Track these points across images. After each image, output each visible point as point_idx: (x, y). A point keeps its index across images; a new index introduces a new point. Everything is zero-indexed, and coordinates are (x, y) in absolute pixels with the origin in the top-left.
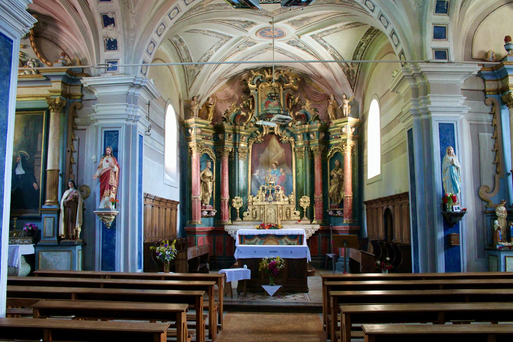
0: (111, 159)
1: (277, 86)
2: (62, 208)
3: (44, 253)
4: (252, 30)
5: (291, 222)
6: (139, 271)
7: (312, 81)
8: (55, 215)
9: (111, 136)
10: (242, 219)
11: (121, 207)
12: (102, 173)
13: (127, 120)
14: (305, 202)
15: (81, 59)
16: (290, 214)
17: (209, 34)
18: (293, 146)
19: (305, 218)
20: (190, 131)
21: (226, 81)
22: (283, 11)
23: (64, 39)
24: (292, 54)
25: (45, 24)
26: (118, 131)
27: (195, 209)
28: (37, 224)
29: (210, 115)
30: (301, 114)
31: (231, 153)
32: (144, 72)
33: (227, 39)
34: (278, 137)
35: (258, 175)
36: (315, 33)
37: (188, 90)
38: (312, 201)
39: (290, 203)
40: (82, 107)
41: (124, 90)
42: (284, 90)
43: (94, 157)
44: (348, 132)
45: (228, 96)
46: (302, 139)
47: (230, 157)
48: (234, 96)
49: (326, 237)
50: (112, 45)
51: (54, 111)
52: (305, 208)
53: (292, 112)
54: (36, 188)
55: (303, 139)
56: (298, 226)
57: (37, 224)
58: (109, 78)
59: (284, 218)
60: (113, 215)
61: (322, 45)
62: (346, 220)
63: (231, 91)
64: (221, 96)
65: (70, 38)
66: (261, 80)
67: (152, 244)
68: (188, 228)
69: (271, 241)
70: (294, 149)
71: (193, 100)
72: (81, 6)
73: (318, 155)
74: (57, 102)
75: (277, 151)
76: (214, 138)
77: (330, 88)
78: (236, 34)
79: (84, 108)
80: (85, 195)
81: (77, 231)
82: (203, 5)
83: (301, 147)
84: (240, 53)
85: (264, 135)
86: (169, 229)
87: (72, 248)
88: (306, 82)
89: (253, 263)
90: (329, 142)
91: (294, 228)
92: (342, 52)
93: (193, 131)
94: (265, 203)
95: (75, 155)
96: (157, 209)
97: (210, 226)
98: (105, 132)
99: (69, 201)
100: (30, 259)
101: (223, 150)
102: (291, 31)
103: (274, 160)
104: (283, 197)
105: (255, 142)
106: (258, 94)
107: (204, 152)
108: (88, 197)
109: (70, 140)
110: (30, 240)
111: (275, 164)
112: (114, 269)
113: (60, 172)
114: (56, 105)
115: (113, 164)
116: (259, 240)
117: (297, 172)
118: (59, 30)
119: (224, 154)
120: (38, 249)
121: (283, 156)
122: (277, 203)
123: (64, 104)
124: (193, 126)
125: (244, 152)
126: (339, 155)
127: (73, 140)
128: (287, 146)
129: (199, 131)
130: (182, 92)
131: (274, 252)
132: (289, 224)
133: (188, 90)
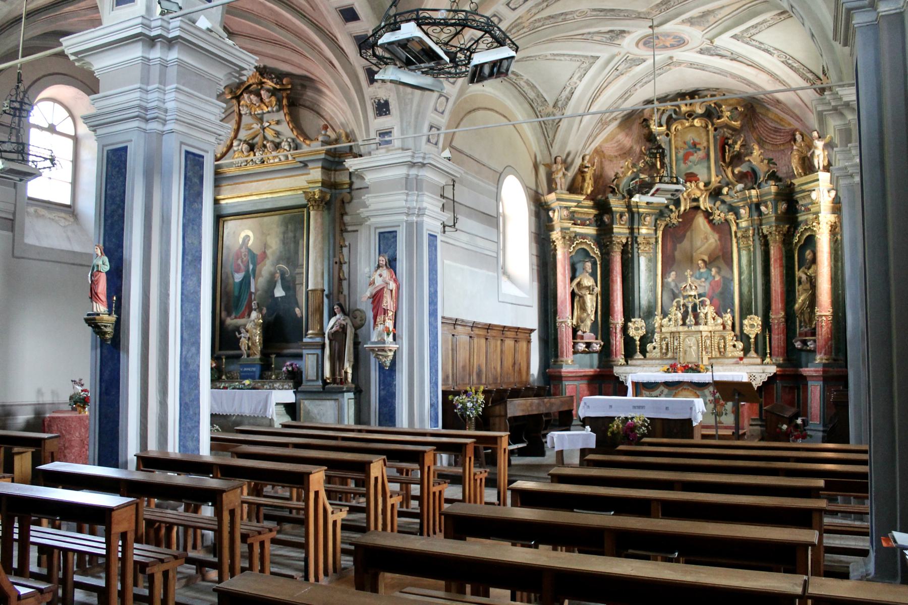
0: (385, 272)
1: (704, 125)
2: (327, 342)
3: (306, 402)
4: (628, 44)
5: (726, 361)
6: (439, 429)
7: (768, 109)
8: (319, 352)
9: (388, 239)
10: (645, 356)
11: (402, 339)
12: (374, 292)
13: (408, 215)
14: (752, 326)
15: (348, 131)
16: (725, 346)
17: (557, 58)
18: (734, 228)
19: (752, 353)
20: (551, 213)
21: (616, 123)
22: (664, 7)
23: (328, 104)
24: (715, 68)
25: (304, 87)
26: (396, 232)
27: (562, 341)
28: (298, 363)
29: (586, 185)
30: (745, 171)
31: (625, 245)
32: (433, 141)
33: (592, 61)
34: (708, 214)
35: (673, 280)
36: (737, 30)
37: (549, 146)
38: (766, 324)
39: (724, 328)
40: (352, 199)
41: (402, 171)
42: (716, 129)
43: (367, 270)
44: (821, 200)
45: (621, 149)
46: (747, 215)
47: (624, 252)
48: (632, 147)
49: (791, 388)
50: (382, 108)
51: (313, 209)
52: (752, 336)
53: (730, 169)
54: (299, 315)
55: (751, 215)
56: (737, 367)
57: (298, 363)
58: (381, 157)
59: (715, 353)
60: (390, 350)
61: (759, 48)
62: (820, 358)
63: (627, 140)
64: (610, 149)
65: (335, 102)
66: (674, 116)
67: (450, 393)
68: (551, 370)
69: (685, 393)
70: (736, 233)
71: (555, 163)
72: (337, 59)
73: (775, 241)
74: (317, 197)
75: (706, 238)
76: (596, 221)
77: (798, 118)
78: (604, 52)
79: (355, 201)
80: (359, 323)
81: (346, 373)
82: (521, 23)
83: (747, 229)
84: (623, 78)
85: (681, 212)
86: (511, 371)
87: (339, 396)
88: (758, 110)
89: (599, 424)
90: (797, 218)
91: (731, 370)
92: (800, 55)
93: (556, 214)
94: (681, 329)
95: (345, 268)
96: (483, 341)
97: (592, 367)
98: (380, 233)
99: (336, 332)
100: (291, 409)
101: (611, 242)
102: (696, 35)
103: (701, 253)
104: (714, 319)
105: (666, 225)
106: (670, 141)
107: (580, 247)
108: (362, 325)
109: (337, 248)
110: (291, 384)
111: (703, 261)
112: (394, 425)
113: (326, 292)
114: (315, 201)
115: (387, 280)
116: (666, 391)
117: (740, 274)
118: (319, 91)
119: (612, 248)
120: (299, 396)
121: (716, 247)
122: (701, 328)
123: (328, 197)
124: (555, 205)
125: (648, 243)
126: (811, 241)
127: (341, 247)
128: (722, 229)
129: (565, 212)
130: (541, 151)
131: (639, 407)
132: (722, 365)
133: (549, 146)
